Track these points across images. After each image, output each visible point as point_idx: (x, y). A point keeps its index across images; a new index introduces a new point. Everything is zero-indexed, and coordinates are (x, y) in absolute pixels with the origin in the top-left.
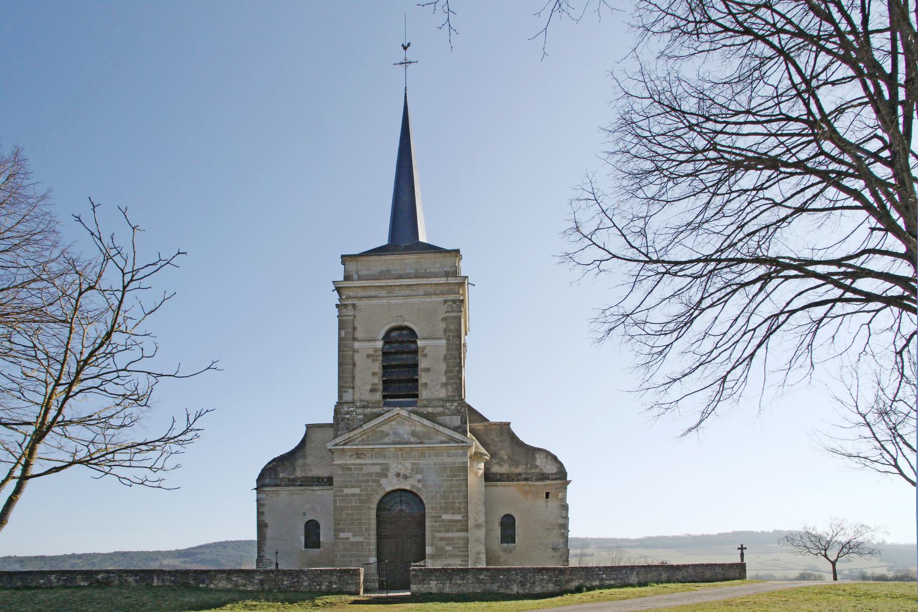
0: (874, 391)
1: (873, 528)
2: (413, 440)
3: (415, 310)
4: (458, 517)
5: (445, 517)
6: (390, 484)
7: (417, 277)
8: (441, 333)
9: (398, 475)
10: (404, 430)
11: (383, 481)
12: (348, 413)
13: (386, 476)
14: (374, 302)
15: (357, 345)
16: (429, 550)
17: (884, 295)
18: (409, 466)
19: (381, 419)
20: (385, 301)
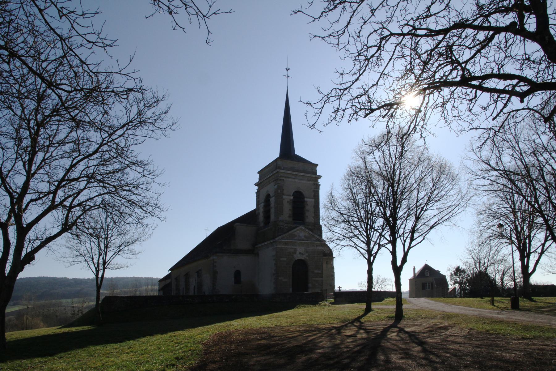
0: (360, 119)
1: (368, 6)
2: (305, 239)
3: (293, 184)
4: (320, 272)
5: (316, 271)
6: (297, 257)
7: (304, 173)
8: (292, 194)
9: (300, 253)
10: (302, 234)
11: (295, 256)
12: (282, 225)
13: (295, 253)
14: (290, 180)
15: (284, 197)
16: (310, 285)
17: (33, 249)
18: (303, 250)
19: (295, 230)
20: (294, 180)
